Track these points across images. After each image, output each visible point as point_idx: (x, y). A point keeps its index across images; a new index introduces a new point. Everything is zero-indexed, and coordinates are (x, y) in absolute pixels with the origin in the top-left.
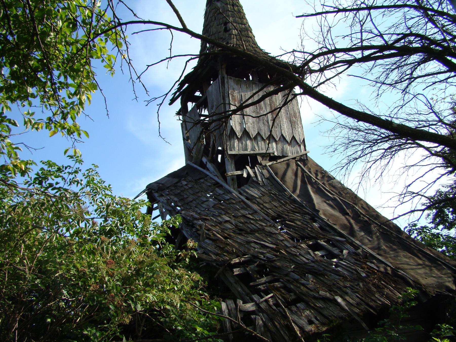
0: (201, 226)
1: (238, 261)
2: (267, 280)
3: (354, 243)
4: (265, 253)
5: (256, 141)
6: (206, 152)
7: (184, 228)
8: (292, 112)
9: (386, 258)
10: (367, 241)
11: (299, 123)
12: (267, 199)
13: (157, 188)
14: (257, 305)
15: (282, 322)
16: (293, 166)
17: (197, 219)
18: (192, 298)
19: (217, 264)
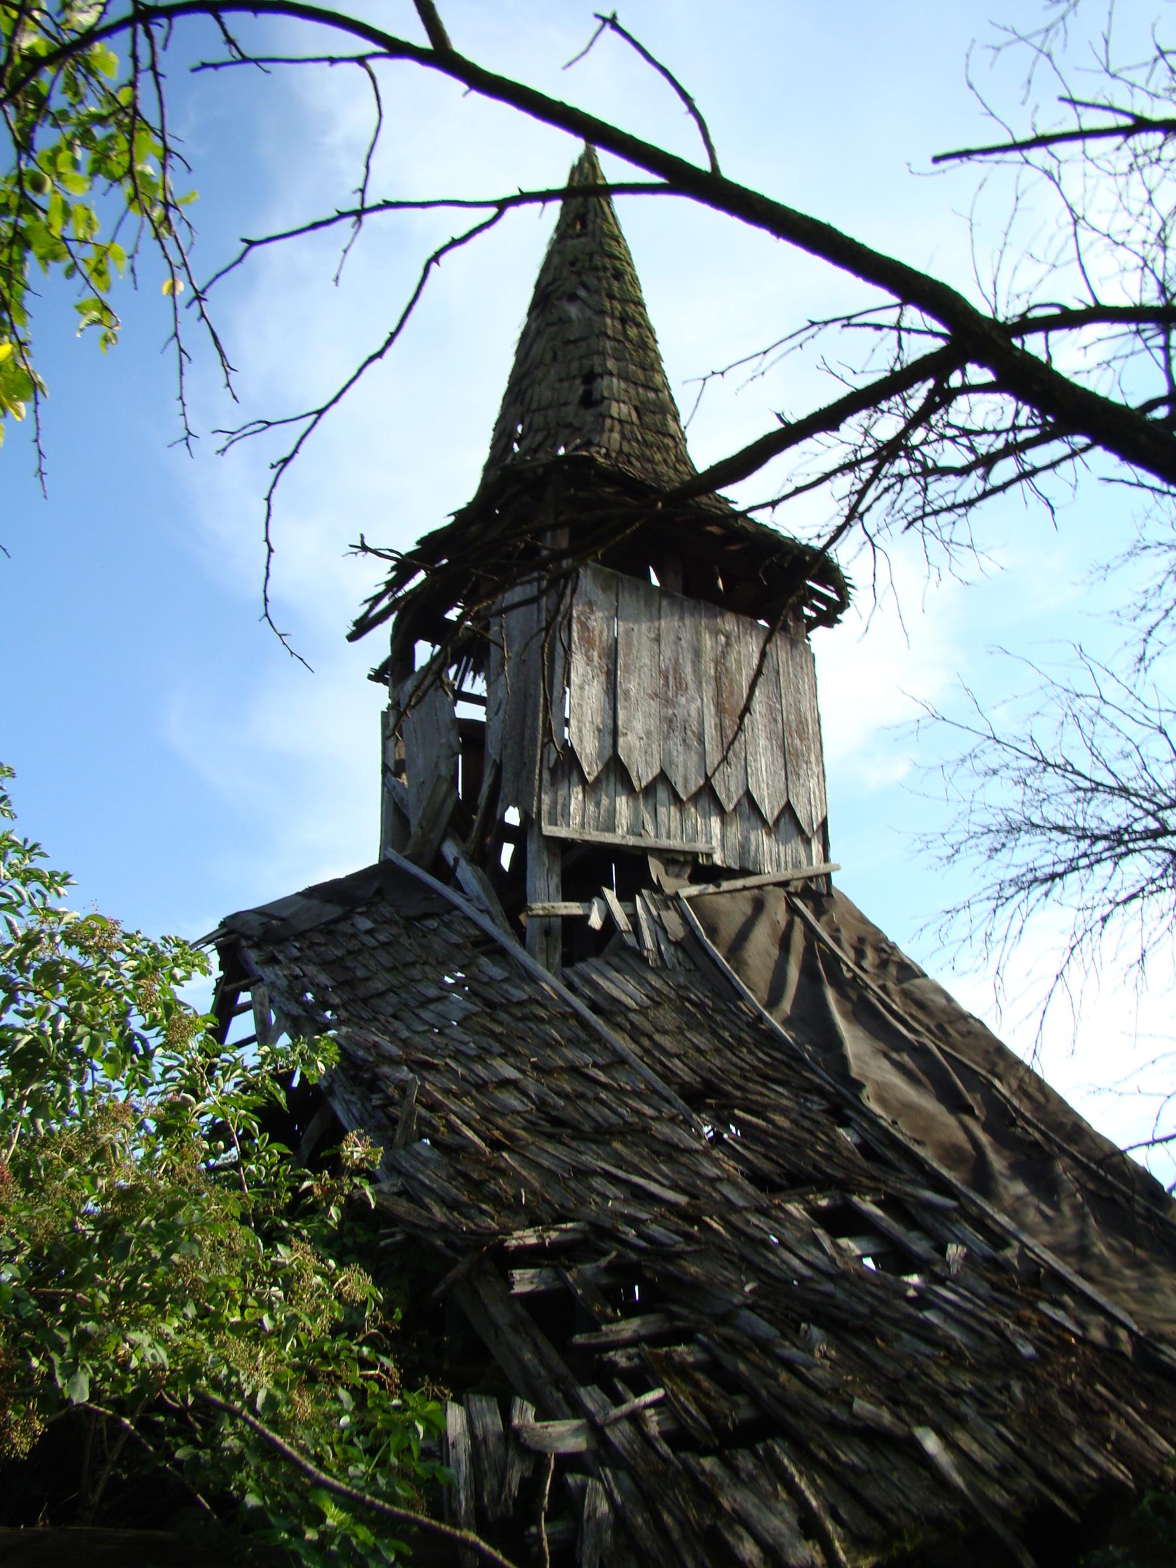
0: (403, 1087)
1: (533, 1240)
2: (643, 1332)
3: (989, 1222)
4: (643, 1222)
5: (650, 802)
6: (458, 825)
7: (338, 1089)
8: (792, 717)
9: (1111, 1291)
10: (1032, 1216)
11: (813, 759)
12: (668, 1017)
13: (258, 932)
14: (596, 1430)
15: (693, 1514)
16: (777, 911)
17: (395, 1062)
18: (329, 1374)
19: (449, 1244)
